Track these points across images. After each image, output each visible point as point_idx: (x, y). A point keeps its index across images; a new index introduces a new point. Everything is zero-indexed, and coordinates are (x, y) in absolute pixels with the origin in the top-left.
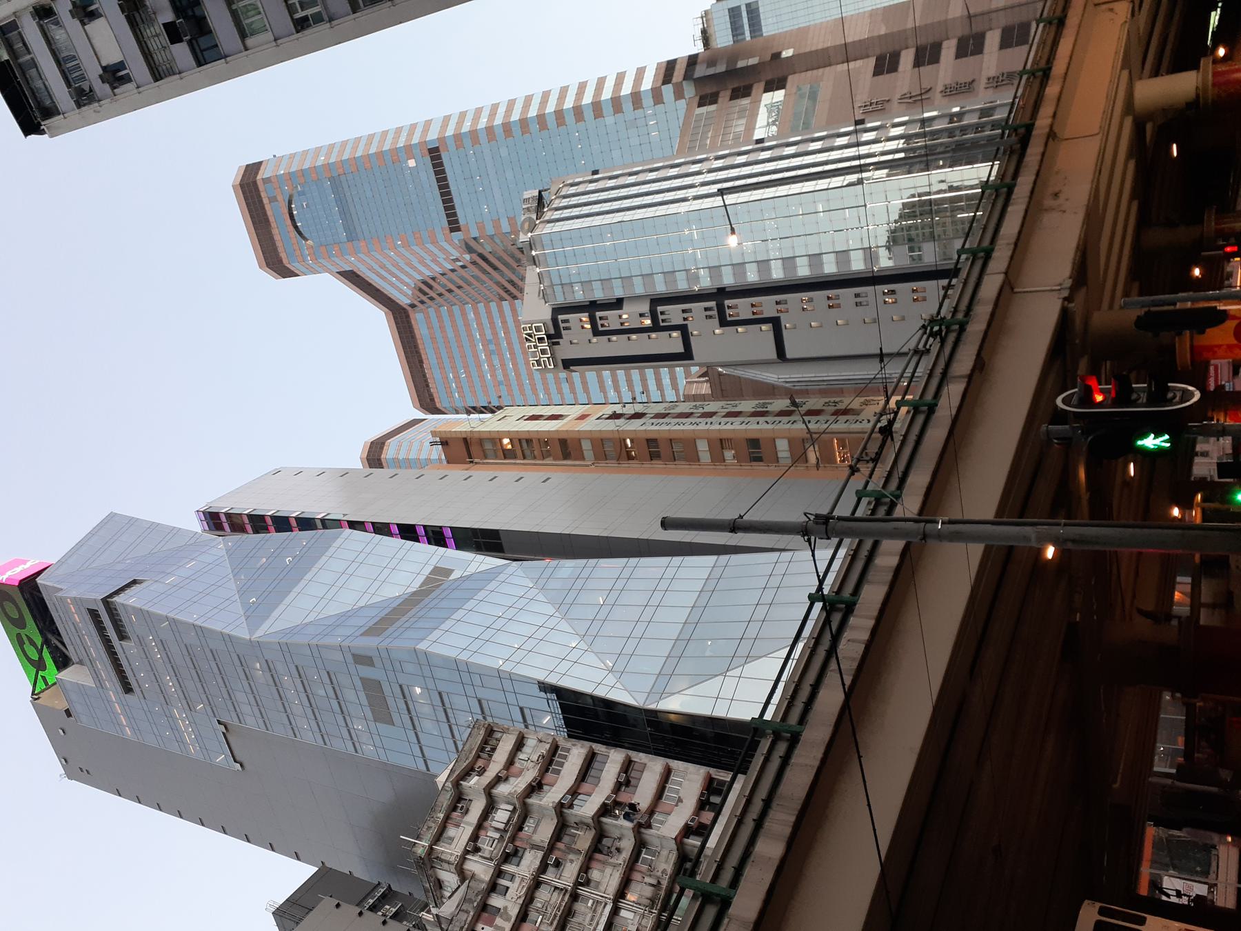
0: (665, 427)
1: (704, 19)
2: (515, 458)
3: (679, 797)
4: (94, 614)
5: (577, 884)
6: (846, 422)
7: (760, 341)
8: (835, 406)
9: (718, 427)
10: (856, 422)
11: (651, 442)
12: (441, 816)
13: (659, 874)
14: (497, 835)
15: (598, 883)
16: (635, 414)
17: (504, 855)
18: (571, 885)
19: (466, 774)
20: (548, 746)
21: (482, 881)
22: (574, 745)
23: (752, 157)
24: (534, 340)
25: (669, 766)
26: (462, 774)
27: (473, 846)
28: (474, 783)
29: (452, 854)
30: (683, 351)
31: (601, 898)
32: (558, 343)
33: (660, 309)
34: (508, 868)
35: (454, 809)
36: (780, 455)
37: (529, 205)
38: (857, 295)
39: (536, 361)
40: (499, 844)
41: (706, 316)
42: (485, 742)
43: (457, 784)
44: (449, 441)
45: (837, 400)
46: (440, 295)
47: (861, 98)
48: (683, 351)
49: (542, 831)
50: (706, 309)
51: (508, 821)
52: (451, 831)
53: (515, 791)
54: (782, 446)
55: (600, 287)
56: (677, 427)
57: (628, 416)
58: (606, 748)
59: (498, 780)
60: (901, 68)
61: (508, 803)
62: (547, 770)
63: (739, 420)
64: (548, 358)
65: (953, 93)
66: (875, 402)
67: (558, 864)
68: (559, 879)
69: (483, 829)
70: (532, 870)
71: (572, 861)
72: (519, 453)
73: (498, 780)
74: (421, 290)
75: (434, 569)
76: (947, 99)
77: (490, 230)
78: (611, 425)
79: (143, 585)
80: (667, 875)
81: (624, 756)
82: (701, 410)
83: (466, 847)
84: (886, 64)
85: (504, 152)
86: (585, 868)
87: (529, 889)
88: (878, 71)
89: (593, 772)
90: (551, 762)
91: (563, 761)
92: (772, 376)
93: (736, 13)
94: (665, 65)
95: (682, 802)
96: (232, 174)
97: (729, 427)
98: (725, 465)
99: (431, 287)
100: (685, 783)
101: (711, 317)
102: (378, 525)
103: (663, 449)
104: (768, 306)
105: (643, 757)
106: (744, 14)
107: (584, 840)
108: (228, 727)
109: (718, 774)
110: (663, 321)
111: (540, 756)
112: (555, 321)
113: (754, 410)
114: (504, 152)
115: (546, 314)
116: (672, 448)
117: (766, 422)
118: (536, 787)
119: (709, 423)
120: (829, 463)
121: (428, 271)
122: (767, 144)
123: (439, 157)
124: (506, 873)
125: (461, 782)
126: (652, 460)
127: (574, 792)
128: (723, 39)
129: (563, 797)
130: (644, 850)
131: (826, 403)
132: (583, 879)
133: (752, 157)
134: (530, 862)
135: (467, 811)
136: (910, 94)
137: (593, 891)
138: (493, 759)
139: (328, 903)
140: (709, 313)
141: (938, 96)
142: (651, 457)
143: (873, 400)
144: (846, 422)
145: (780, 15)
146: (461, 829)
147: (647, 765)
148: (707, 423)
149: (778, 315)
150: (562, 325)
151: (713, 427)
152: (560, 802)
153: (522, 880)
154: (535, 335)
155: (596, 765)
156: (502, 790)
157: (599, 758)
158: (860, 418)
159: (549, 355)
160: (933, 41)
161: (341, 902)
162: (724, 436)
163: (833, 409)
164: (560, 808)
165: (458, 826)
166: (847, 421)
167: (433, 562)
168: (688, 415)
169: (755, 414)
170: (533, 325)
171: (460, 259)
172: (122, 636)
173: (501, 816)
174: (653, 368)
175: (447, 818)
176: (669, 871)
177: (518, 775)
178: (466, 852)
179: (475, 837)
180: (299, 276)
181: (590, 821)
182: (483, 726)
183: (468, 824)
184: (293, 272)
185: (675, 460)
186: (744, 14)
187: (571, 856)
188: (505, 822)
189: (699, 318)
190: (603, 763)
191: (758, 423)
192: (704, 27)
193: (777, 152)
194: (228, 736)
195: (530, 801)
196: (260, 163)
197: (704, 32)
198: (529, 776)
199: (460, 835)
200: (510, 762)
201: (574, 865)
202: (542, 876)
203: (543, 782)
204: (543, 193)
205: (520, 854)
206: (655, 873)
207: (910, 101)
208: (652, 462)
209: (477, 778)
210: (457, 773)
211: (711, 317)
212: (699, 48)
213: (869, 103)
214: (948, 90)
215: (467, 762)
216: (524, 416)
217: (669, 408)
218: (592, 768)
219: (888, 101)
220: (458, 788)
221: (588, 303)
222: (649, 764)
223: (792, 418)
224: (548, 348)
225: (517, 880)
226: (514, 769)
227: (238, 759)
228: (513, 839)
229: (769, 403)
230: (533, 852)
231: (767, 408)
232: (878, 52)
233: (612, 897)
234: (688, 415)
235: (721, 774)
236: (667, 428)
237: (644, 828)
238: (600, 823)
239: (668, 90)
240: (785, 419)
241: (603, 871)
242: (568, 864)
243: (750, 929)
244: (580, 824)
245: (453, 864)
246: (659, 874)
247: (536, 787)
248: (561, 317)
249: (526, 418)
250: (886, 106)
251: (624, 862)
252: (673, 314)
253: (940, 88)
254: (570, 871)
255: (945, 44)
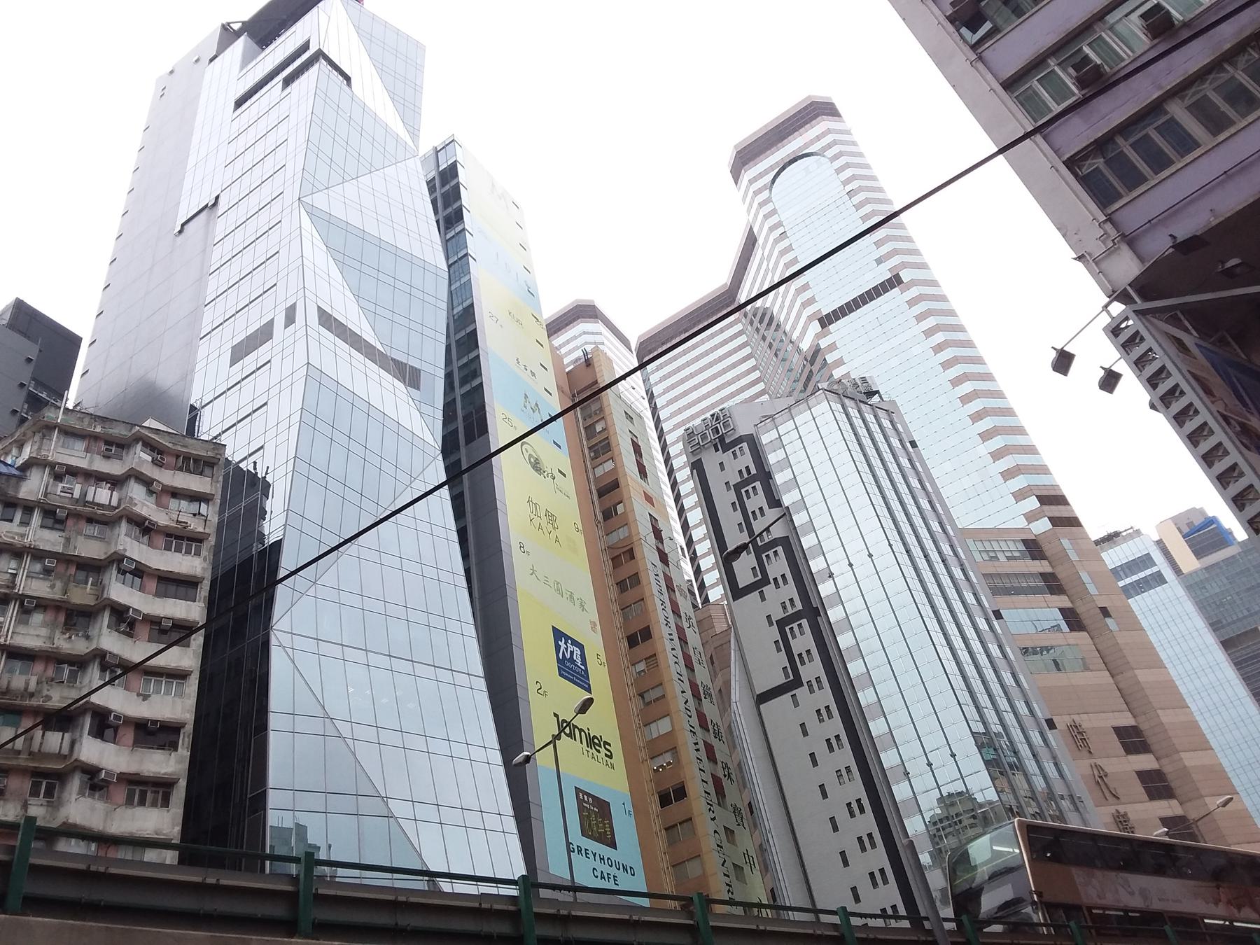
0: (655, 589)
1: (1131, 531)
2: (588, 439)
3: (149, 696)
4: (305, 47)
5: (21, 598)
6: (706, 792)
7: (771, 672)
8: (725, 776)
9: (668, 648)
10: (708, 804)
11: (635, 579)
12: (98, 429)
13: (45, 693)
14: (77, 494)
15: (26, 623)
16: (666, 555)
17: (52, 508)
18: (20, 593)
19: (150, 446)
20: (200, 529)
21: (17, 490)
22: (205, 559)
23: (976, 611)
24: (713, 424)
25: (190, 675)
26: (153, 443)
27: (61, 473)
28: (140, 458)
29: (49, 450)
30: (740, 587)
31: (6, 630)
32: (717, 450)
33: (780, 549)
34: (36, 518)
35: (108, 443)
36: (653, 726)
37: (860, 384)
38: (848, 769)
39: (693, 432)
40: (67, 500)
41: (784, 602)
42: (197, 460)
43: (138, 439)
44: (591, 366)
45: (733, 777)
46: (764, 338)
47: (1086, 722)
48: (740, 587)
49: (89, 548)
50: (791, 600)
51: (98, 505)
52: (80, 446)
53: (136, 504)
54: (663, 726)
55: (787, 479)
56: (658, 603)
57: (661, 547)
58: (205, 597)
59: (147, 482)
60: (1132, 758)
61: (120, 500)
62: (169, 535)
63: (684, 671)
64: (699, 443)
65: (1120, 826)
66: (740, 821)
67: (47, 572)
68: (27, 577)
69: (85, 478)
70: (37, 543)
71: (52, 587)
72: (594, 441)
73: (147, 482)
74: (763, 315)
75: (416, 369)
76: (1112, 820)
77: (830, 358)
78: (645, 529)
79: (346, 88)
80: (43, 702)
81: (197, 619)
82: (686, 625)
83: (59, 463)
84: (1132, 740)
85: (917, 350)
86: (42, 605)
87: (11, 544)
88: (1120, 731)
89: (172, 588)
90: (180, 538)
91: (183, 551)
92: (737, 693)
93: (1147, 562)
94: (1058, 493)
95: (143, 700)
96: (821, 92)
97: (671, 660)
98: (628, 667)
99: (770, 324)
100: (169, 698)
101: (784, 608)
102: (471, 310)
103: (631, 594)
104: (813, 669)
105: (198, 642)
106: (1148, 572)
107: (82, 595)
108: (215, 208)
109: (186, 735)
110: (768, 556)
111: (187, 523)
112: (740, 440)
113: (700, 685)
114: (917, 350)
115: (744, 429)
116: (634, 604)
117: (687, 702)
118: (145, 528)
119: (671, 637)
120: (655, 784)
121: (777, 311)
122: (995, 623)
123: (893, 287)
124: (31, 514)
125: (140, 443)
126: (617, 584)
127: (140, 572)
128: (1113, 557)
129: (132, 559)
130: (75, 668)
131: (726, 764)
132: (29, 606)
133: (976, 611)
134: (50, 540)
135: (107, 457)
136: (1106, 776)
137: (14, 619)
138: (176, 472)
139: (32, 350)
140: (788, 604)
141: (1112, 809)
142: (619, 582)
143: (742, 818)
144: (706, 792)
145: (1193, 638)
146: (82, 454)
147: (187, 649)
148: (671, 634)
149: (805, 684)
150: (737, 448)
151: (667, 643)
152: (124, 557)
153: (23, 536)
154: (719, 423)
155: (182, 590)
156: (136, 491)
157: (191, 591)
158: (716, 807)
159: (702, 444)
160: (1173, 787)
161: (33, 364)
162: (660, 657)
163: (720, 774)
164: (117, 560)
165: (87, 450)
166: (709, 794)
167: (424, 367)
168: (676, 612)
169: (694, 686)
170: (729, 419)
171: (1046, 547)
172: (288, 82)
173: (103, 495)
174: (716, 562)
175: (95, 437)
176: (49, 704)
177: (159, 504)
178: (52, 465)
179: (73, 472)
180: (736, 185)
181: (105, 596)
182: (217, 454)
183: (91, 462)
184: (738, 180)
185: (622, 610)
186: (1148, 572)
187: (59, 585)
188: (96, 501)
189: (783, 596)
190: (124, 581)
191: (683, 692)
192: (1121, 532)
193: (988, 636)
194: (206, 210)
195: (124, 524)
196: (839, 116)
197: (1117, 534)
198: (161, 518)
199: (76, 455)
200: (176, 493)
201: (48, 590)
202: (29, 559)
203: (152, 533)
204: (877, 395)
205: (57, 526)
206: (45, 686)
207: (1096, 777)
208: (615, 586)
209: (150, 459)
210: (154, 436)
211: (784, 608)
212: (1094, 529)
213: (1081, 730)
214: (1122, 820)
215: (170, 445)
216: (637, 437)
217: (681, 590)
218: (178, 586)
219: (1090, 752)
220: (134, 440)
221: (767, 470)
222: (190, 651)
223: (698, 729)
224: (710, 440)
225: (22, 530)
226: (165, 499)
227: (185, 227)
228: (77, 516)
229: (711, 699)
230: (62, 540)
231: (705, 698)
232: (1143, 727)
233: (8, 643)
234: (676, 612)
235: (186, 739)
236: (655, 592)
237: (101, 661)
238: (104, 608)
239: (1032, 503)
240: (695, 721)
241: (42, 626)
242: (48, 584)
243: (4, 819)
244: (100, 587)
245: (38, 455)
246: (45, 693)
247: (145, 528)
248: (745, 445)
249: (635, 439)
250: (1085, 753)
251: (57, 648)
252: (778, 566)
253: (1122, 809)
254: (40, 588)
255: (1174, 802)
